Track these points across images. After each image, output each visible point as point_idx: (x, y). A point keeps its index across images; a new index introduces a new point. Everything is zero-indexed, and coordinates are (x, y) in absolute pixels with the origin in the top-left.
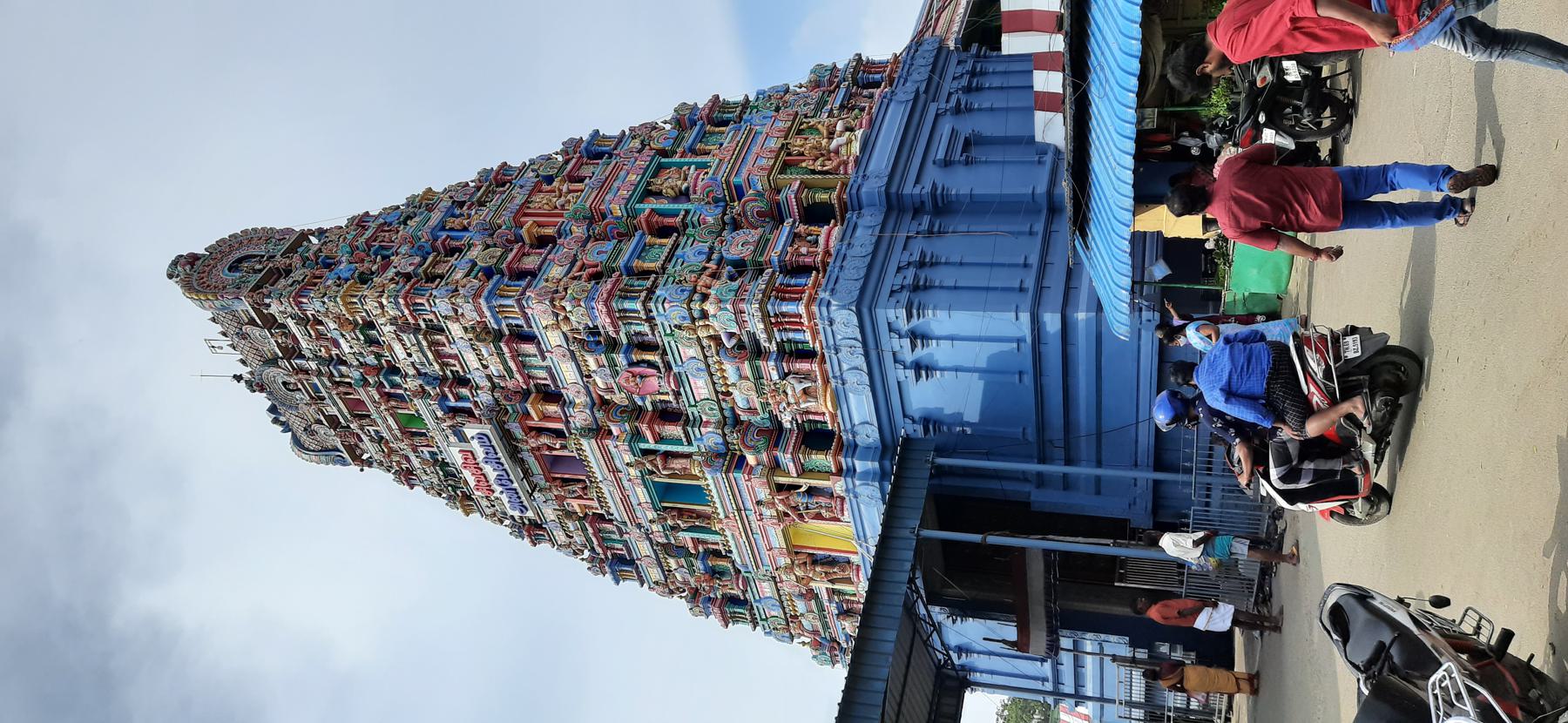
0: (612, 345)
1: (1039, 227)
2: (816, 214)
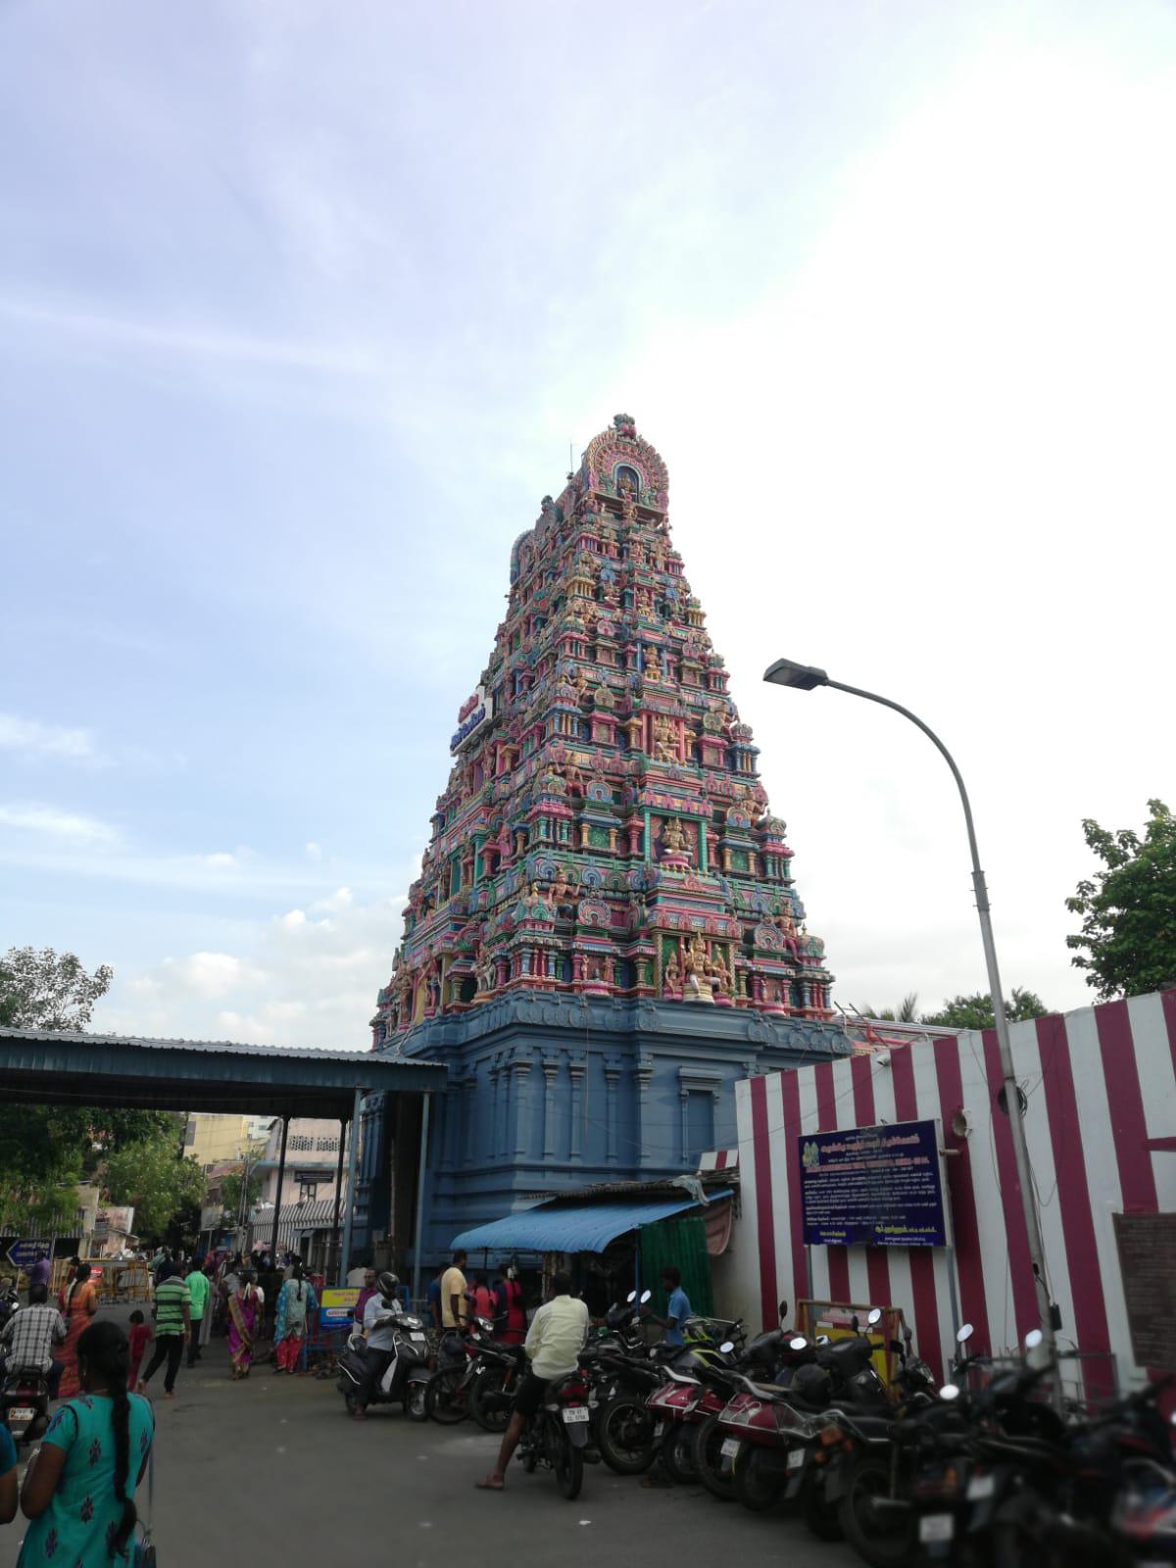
1: (613, 1164)
2: (628, 969)
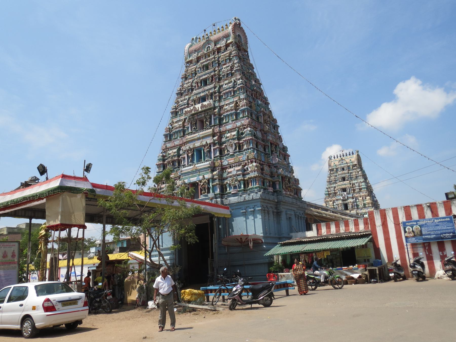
0: (239, 139)
